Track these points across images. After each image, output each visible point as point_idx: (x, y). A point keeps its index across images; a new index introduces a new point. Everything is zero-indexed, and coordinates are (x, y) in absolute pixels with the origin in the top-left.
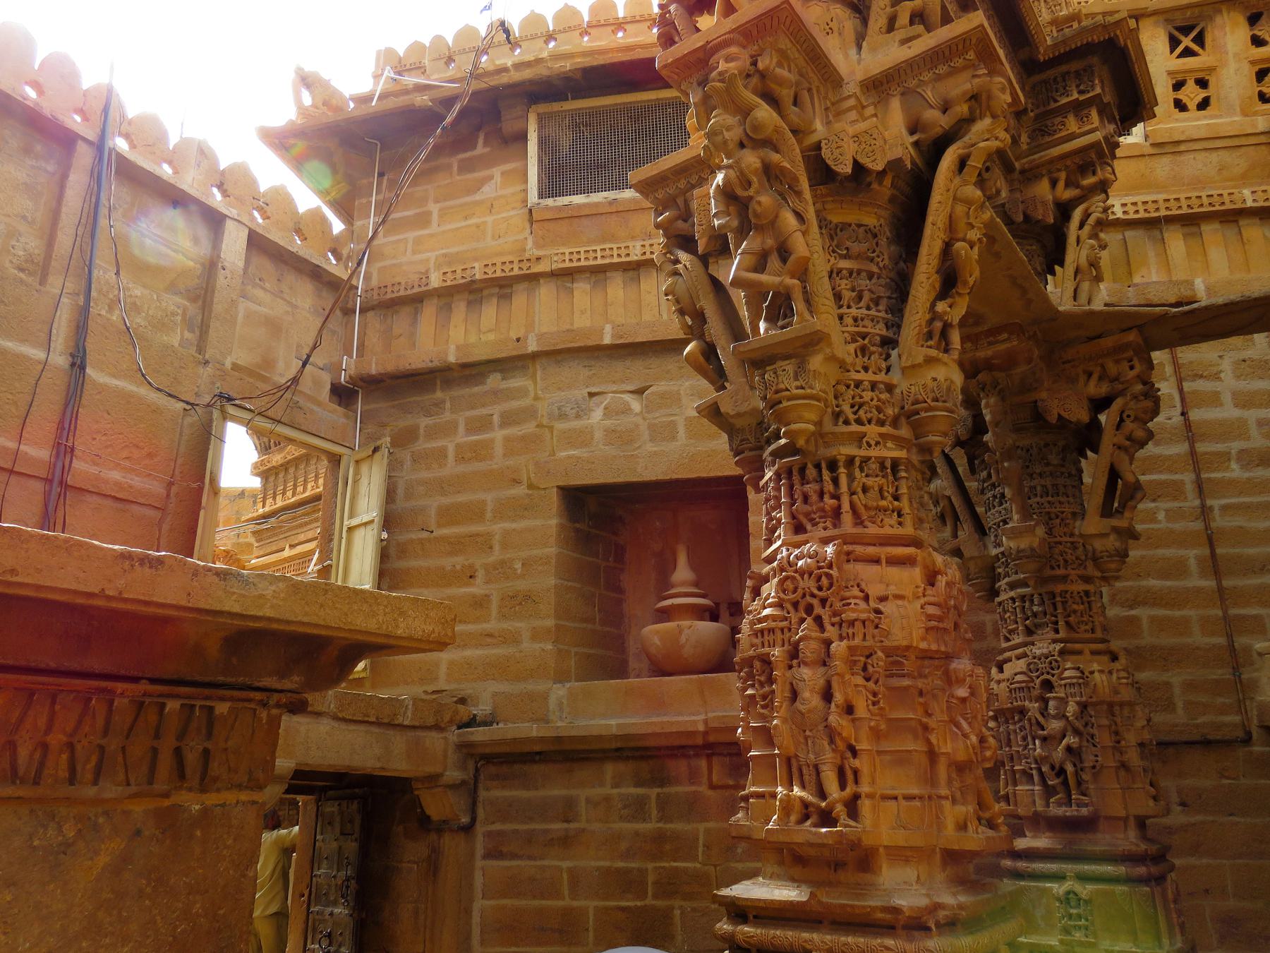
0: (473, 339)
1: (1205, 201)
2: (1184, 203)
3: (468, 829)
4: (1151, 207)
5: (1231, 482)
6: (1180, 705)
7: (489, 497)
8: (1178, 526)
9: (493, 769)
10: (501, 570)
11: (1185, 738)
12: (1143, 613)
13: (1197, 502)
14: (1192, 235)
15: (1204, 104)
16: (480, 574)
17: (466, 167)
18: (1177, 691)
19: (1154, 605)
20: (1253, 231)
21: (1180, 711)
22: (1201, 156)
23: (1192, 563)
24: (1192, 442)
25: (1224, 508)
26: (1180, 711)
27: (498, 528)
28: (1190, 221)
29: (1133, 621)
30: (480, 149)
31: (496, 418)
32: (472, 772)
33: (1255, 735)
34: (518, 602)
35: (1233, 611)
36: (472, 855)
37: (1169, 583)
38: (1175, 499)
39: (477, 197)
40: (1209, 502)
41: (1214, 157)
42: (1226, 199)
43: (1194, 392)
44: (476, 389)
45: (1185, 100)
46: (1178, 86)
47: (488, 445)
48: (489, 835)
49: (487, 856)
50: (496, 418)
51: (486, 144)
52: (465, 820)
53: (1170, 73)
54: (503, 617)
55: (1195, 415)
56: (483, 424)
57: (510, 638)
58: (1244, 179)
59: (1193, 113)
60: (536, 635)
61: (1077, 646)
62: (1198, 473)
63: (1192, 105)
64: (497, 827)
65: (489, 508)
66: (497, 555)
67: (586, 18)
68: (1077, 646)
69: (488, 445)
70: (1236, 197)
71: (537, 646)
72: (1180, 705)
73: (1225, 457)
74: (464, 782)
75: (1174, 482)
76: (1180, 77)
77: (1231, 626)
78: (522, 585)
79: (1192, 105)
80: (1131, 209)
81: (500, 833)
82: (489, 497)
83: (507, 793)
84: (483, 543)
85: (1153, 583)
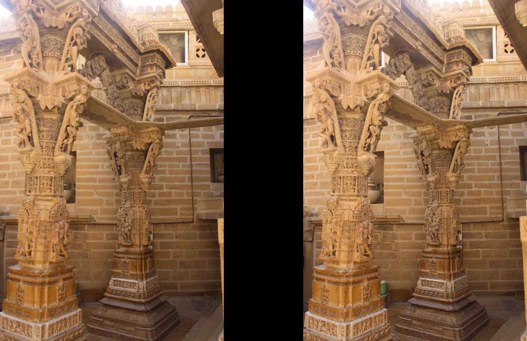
0: (7, 110)
1: (505, 79)
2: (505, 79)
3: (312, 242)
4: (188, 83)
5: (508, 156)
6: (488, 213)
7: (10, 154)
8: (184, 169)
9: (9, 226)
10: (12, 175)
11: (179, 221)
12: (482, 189)
13: (190, 163)
14: (198, 91)
15: (198, 56)
16: (7, 175)
17: (8, 59)
18: (488, 209)
19: (485, 188)
20: (522, 88)
21: (488, 214)
22: (510, 66)
23: (496, 177)
24: (500, 145)
25: (505, 163)
26: (488, 214)
27: (11, 163)
28: (506, 83)
29: (171, 193)
30: (12, 54)
31: (12, 133)
32: (312, 228)
33: (505, 220)
34: (16, 184)
35: (504, 189)
36: (313, 247)
37: (489, 182)
38: (494, 160)
39: (10, 69)
40: (502, 161)
41: (514, 67)
42: (515, 78)
43: (502, 132)
44: (7, 124)
45: (507, 50)
46: (198, 50)
47: (10, 140)
48: (8, 242)
49: (7, 247)
50: (12, 133)
51: (13, 53)
52: (311, 239)
53: (504, 42)
54: (12, 187)
55: (501, 138)
56: (9, 134)
57: (14, 193)
58: (212, 77)
59: (509, 53)
60: (20, 192)
61: (443, 205)
62: (191, 155)
63: (201, 56)
64: (10, 240)
65: (10, 157)
66: (11, 171)
67: (461, 7)
68: (443, 205)
69: (10, 140)
70: (518, 78)
71: (20, 195)
72: (488, 213)
73: (198, 151)
74: (310, 230)
75: (185, 158)
76: (198, 48)
77: (193, 194)
78: (17, 179)
79: (201, 56)
80: (183, 83)
81: (11, 242)
82: (10, 154)
83: (12, 232)
84: (8, 167)
85: (177, 183)
